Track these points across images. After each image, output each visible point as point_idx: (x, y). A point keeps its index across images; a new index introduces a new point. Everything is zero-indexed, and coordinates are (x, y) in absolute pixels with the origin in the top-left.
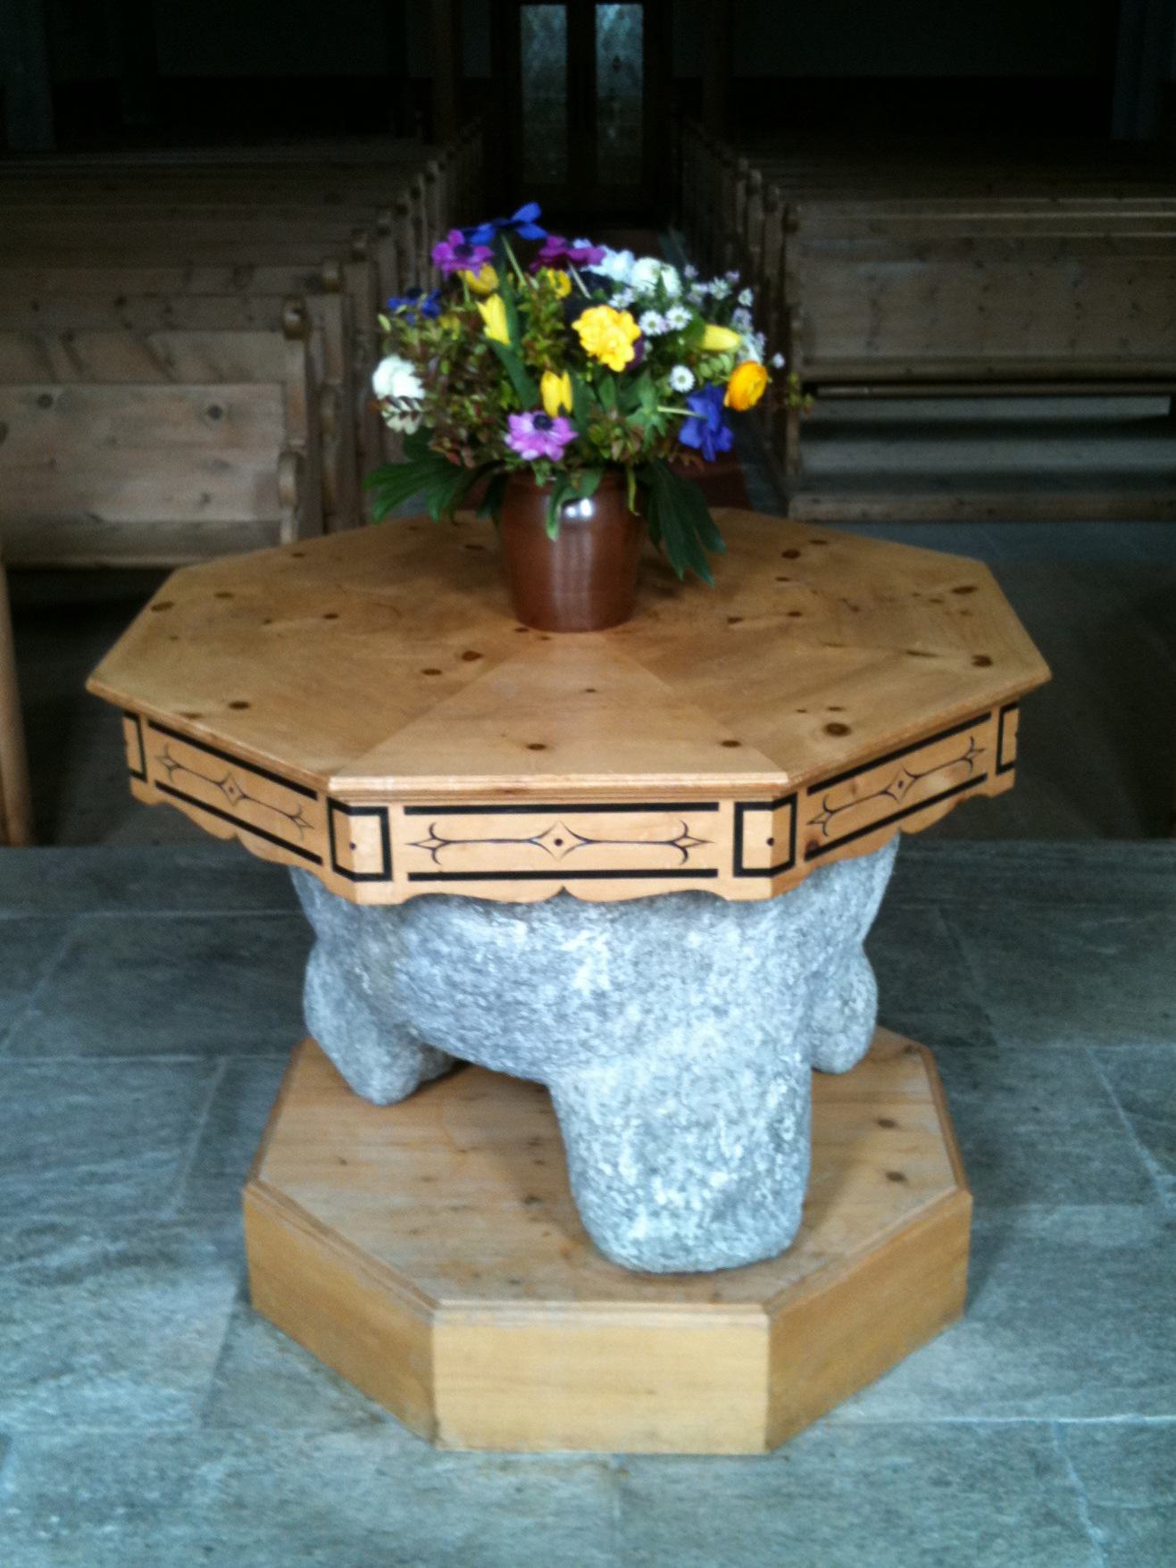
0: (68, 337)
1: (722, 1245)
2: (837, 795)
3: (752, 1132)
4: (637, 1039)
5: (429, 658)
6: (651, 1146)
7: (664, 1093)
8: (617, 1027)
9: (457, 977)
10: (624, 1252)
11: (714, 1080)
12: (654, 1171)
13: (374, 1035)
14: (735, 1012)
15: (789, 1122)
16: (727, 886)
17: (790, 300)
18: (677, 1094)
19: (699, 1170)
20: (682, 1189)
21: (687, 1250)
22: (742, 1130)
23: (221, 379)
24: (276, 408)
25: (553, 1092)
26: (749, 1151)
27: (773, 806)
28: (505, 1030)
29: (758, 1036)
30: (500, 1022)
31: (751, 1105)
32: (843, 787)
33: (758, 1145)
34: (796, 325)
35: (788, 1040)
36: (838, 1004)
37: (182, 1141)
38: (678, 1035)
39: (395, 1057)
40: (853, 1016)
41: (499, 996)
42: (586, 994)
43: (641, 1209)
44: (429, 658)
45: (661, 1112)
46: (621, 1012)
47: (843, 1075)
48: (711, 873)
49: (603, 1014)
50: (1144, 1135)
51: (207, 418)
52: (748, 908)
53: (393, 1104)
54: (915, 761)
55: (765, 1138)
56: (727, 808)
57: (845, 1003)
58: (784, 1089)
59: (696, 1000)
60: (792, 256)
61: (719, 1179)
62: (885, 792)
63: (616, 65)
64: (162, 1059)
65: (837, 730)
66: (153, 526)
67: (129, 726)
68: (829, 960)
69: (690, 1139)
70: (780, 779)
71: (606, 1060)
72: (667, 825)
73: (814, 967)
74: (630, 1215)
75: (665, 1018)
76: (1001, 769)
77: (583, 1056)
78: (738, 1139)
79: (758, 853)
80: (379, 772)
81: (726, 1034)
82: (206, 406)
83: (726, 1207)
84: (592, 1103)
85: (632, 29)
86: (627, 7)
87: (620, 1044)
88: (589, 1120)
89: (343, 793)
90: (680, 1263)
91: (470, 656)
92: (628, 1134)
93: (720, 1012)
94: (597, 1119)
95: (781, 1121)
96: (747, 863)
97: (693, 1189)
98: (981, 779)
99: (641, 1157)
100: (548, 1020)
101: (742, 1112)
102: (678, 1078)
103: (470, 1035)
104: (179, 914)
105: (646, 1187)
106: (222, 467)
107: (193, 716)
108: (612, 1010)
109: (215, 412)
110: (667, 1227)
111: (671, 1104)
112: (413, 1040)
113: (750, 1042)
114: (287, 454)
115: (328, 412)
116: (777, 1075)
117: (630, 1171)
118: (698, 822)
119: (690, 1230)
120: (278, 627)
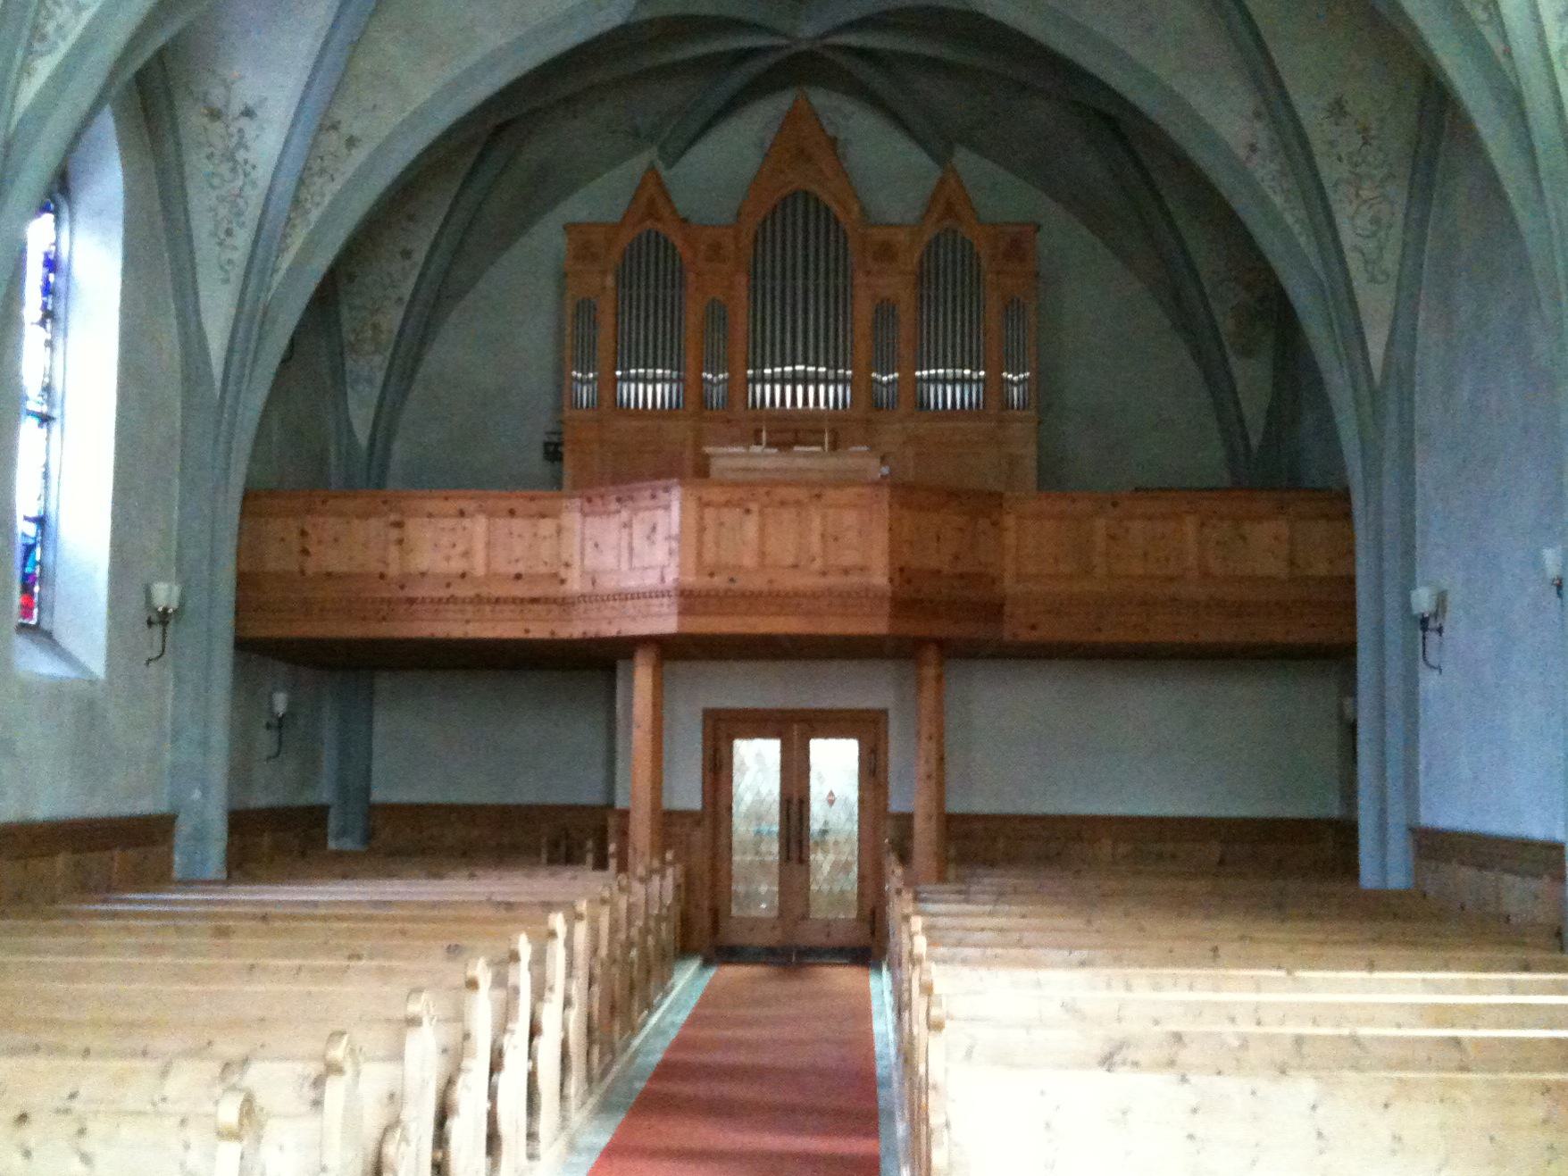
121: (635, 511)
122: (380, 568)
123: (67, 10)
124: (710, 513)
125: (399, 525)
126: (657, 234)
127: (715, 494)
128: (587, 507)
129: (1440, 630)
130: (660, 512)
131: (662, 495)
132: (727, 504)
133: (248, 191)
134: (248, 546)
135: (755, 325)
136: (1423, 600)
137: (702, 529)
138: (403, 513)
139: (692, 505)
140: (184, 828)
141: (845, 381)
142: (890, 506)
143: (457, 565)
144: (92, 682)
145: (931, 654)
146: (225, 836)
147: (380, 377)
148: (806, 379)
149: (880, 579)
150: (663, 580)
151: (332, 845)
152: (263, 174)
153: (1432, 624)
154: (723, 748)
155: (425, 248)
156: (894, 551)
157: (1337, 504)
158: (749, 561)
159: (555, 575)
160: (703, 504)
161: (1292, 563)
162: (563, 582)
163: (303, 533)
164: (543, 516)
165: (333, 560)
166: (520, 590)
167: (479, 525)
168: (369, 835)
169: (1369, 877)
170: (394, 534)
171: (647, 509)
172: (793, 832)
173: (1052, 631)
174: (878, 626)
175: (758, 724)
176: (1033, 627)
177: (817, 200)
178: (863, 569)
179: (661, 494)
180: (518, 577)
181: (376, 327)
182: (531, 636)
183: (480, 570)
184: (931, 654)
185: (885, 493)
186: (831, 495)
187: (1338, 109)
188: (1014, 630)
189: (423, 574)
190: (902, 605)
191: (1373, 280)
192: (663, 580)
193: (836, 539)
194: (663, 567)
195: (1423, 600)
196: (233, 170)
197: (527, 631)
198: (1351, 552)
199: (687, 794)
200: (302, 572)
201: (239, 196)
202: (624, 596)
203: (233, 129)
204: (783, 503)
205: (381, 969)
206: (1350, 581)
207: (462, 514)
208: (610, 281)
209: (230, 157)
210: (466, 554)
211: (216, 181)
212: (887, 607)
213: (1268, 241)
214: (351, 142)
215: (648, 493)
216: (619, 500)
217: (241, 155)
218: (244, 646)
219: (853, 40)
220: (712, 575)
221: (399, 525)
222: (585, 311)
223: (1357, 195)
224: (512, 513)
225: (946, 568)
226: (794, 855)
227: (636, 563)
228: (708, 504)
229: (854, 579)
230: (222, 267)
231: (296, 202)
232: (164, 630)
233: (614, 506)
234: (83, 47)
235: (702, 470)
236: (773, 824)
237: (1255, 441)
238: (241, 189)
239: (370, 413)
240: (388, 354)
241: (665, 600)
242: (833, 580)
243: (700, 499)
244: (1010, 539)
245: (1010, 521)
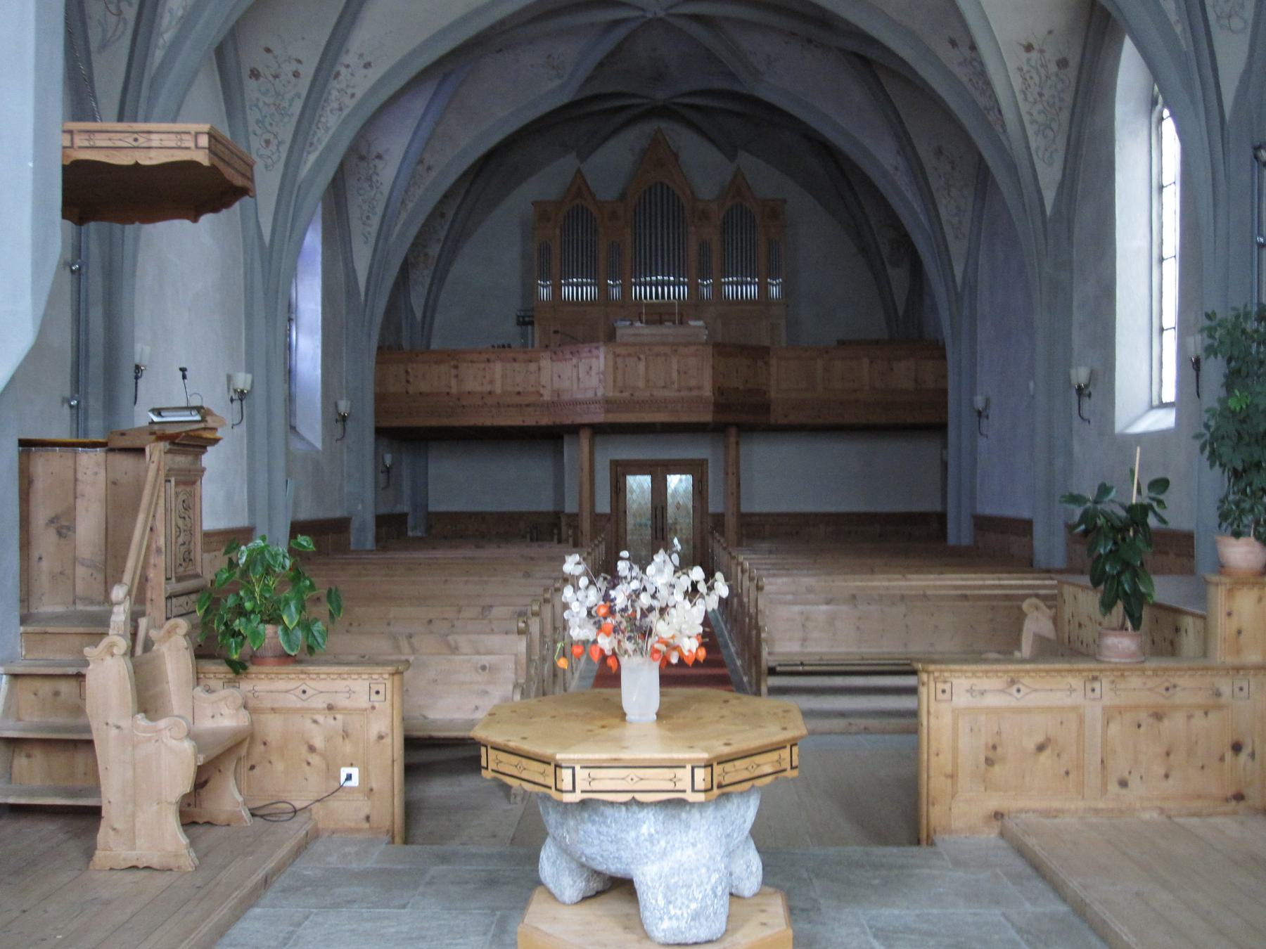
0: (410, 636)
1: (694, 931)
2: (728, 766)
3: (706, 890)
4: (664, 854)
5: (590, 727)
6: (669, 894)
7: (674, 874)
8: (657, 849)
9: (601, 830)
10: (660, 935)
11: (691, 870)
12: (670, 902)
13: (567, 873)
14: (699, 846)
15: (720, 889)
16: (690, 797)
17: (761, 623)
18: (679, 874)
19: (686, 902)
20: (680, 909)
21: (682, 933)
22: (702, 889)
23: (478, 653)
24: (512, 666)
25: (637, 886)
26: (704, 897)
27: (705, 767)
28: (618, 850)
29: (708, 856)
30: (615, 847)
31: (705, 880)
32: (730, 764)
33: (708, 895)
34: (763, 635)
35: (719, 858)
36: (745, 867)
37: (485, 934)
38: (679, 852)
39: (575, 882)
40: (751, 873)
41: (616, 836)
42: (646, 834)
43: (666, 917)
44: (590, 727)
45: (673, 881)
46: (658, 843)
47: (749, 898)
48: (684, 791)
49: (652, 844)
50: (875, 936)
51: (480, 671)
52: (701, 805)
53: (577, 903)
54: (758, 759)
55: (710, 893)
56: (689, 767)
57: (748, 867)
58: (717, 876)
59: (685, 839)
60: (761, 602)
61: (694, 906)
62: (747, 769)
63: (678, 507)
64: (474, 911)
65: (727, 744)
66: (451, 721)
67: (483, 750)
68: (733, 830)
69: (683, 891)
70: (706, 756)
71: (653, 862)
72: (668, 773)
73: (728, 832)
74: (661, 919)
75: (674, 846)
76: (792, 768)
77: (645, 860)
78: (700, 892)
79: (700, 784)
80: (575, 752)
81: (696, 854)
82: (479, 666)
83: (695, 916)
84: (648, 878)
85: (687, 488)
86: (684, 477)
87: (658, 856)
88: (647, 884)
89: (562, 760)
90: (679, 939)
91: (603, 727)
92: (661, 889)
93: (694, 845)
94: (650, 883)
95: (717, 888)
96: (696, 788)
97: (684, 909)
98: (784, 770)
99: (665, 897)
100: (633, 845)
101: (702, 883)
102: (679, 869)
103: (605, 854)
104: (474, 868)
105: (667, 908)
106: (486, 693)
107: (509, 741)
108: (655, 842)
109: (484, 668)
110: (675, 923)
111: (676, 878)
112: (582, 865)
113: (705, 857)
114: (516, 685)
115: (533, 671)
116: (715, 871)
117: (661, 902)
118: (679, 772)
119: (683, 924)
120: (534, 720)
121: (581, 359)
122: (448, 390)
123: (323, 131)
124: (620, 360)
125: (456, 367)
126: (582, 207)
127: (620, 350)
128: (554, 357)
129: (987, 417)
130: (594, 360)
131: (595, 352)
132: (630, 355)
133: (378, 196)
134: (380, 381)
135: (635, 253)
136: (979, 402)
137: (616, 368)
138: (457, 360)
139: (610, 357)
140: (355, 525)
141: (684, 284)
142: (713, 356)
143: (487, 388)
144: (318, 452)
145: (733, 431)
146: (374, 528)
147: (428, 280)
148: (663, 284)
149: (707, 392)
150: (596, 394)
151: (410, 534)
152: (386, 189)
153: (984, 414)
154: (621, 480)
155: (452, 213)
156: (714, 381)
157: (937, 351)
158: (641, 384)
159: (538, 392)
160: (616, 355)
161: (916, 381)
162: (542, 395)
163: (407, 372)
164: (530, 361)
165: (424, 387)
166: (518, 400)
167: (498, 367)
168: (429, 528)
169: (952, 540)
170: (453, 372)
171: (586, 358)
172: (659, 525)
173: (794, 418)
174: (707, 417)
175: (639, 467)
176: (786, 416)
177: (668, 187)
178: (699, 388)
179: (593, 350)
180: (519, 393)
181: (426, 255)
182: (526, 424)
183: (498, 390)
184: (733, 431)
185: (710, 350)
186: (682, 350)
187: (939, 152)
188: (777, 417)
189: (469, 393)
190: (719, 407)
191: (957, 237)
192: (596, 394)
193: (685, 373)
194: (596, 389)
195: (979, 402)
196: (371, 186)
197: (524, 421)
198: (945, 377)
199: (603, 506)
200: (407, 393)
201: (373, 199)
202: (576, 403)
203: (371, 165)
204: (658, 355)
205: (503, 582)
206: (944, 392)
207: (488, 361)
208: (558, 231)
209: (369, 179)
210: (492, 382)
211: (362, 192)
212: (711, 407)
213: (907, 220)
214: (429, 168)
215: (586, 349)
216: (572, 353)
217: (375, 178)
218: (381, 432)
219: (687, 100)
220: (621, 392)
221: (456, 367)
222: (545, 250)
223: (949, 195)
224: (515, 360)
225: (741, 387)
226: (659, 535)
227: (581, 385)
228: (619, 355)
229: (695, 393)
230: (364, 235)
231: (403, 202)
232: (344, 425)
233: (568, 356)
234: (329, 148)
235: (611, 337)
236: (646, 519)
237: (901, 311)
238: (375, 195)
239: (423, 301)
240: (432, 268)
241: (598, 406)
242: (684, 393)
243: (614, 353)
244: (773, 370)
245: (773, 362)
